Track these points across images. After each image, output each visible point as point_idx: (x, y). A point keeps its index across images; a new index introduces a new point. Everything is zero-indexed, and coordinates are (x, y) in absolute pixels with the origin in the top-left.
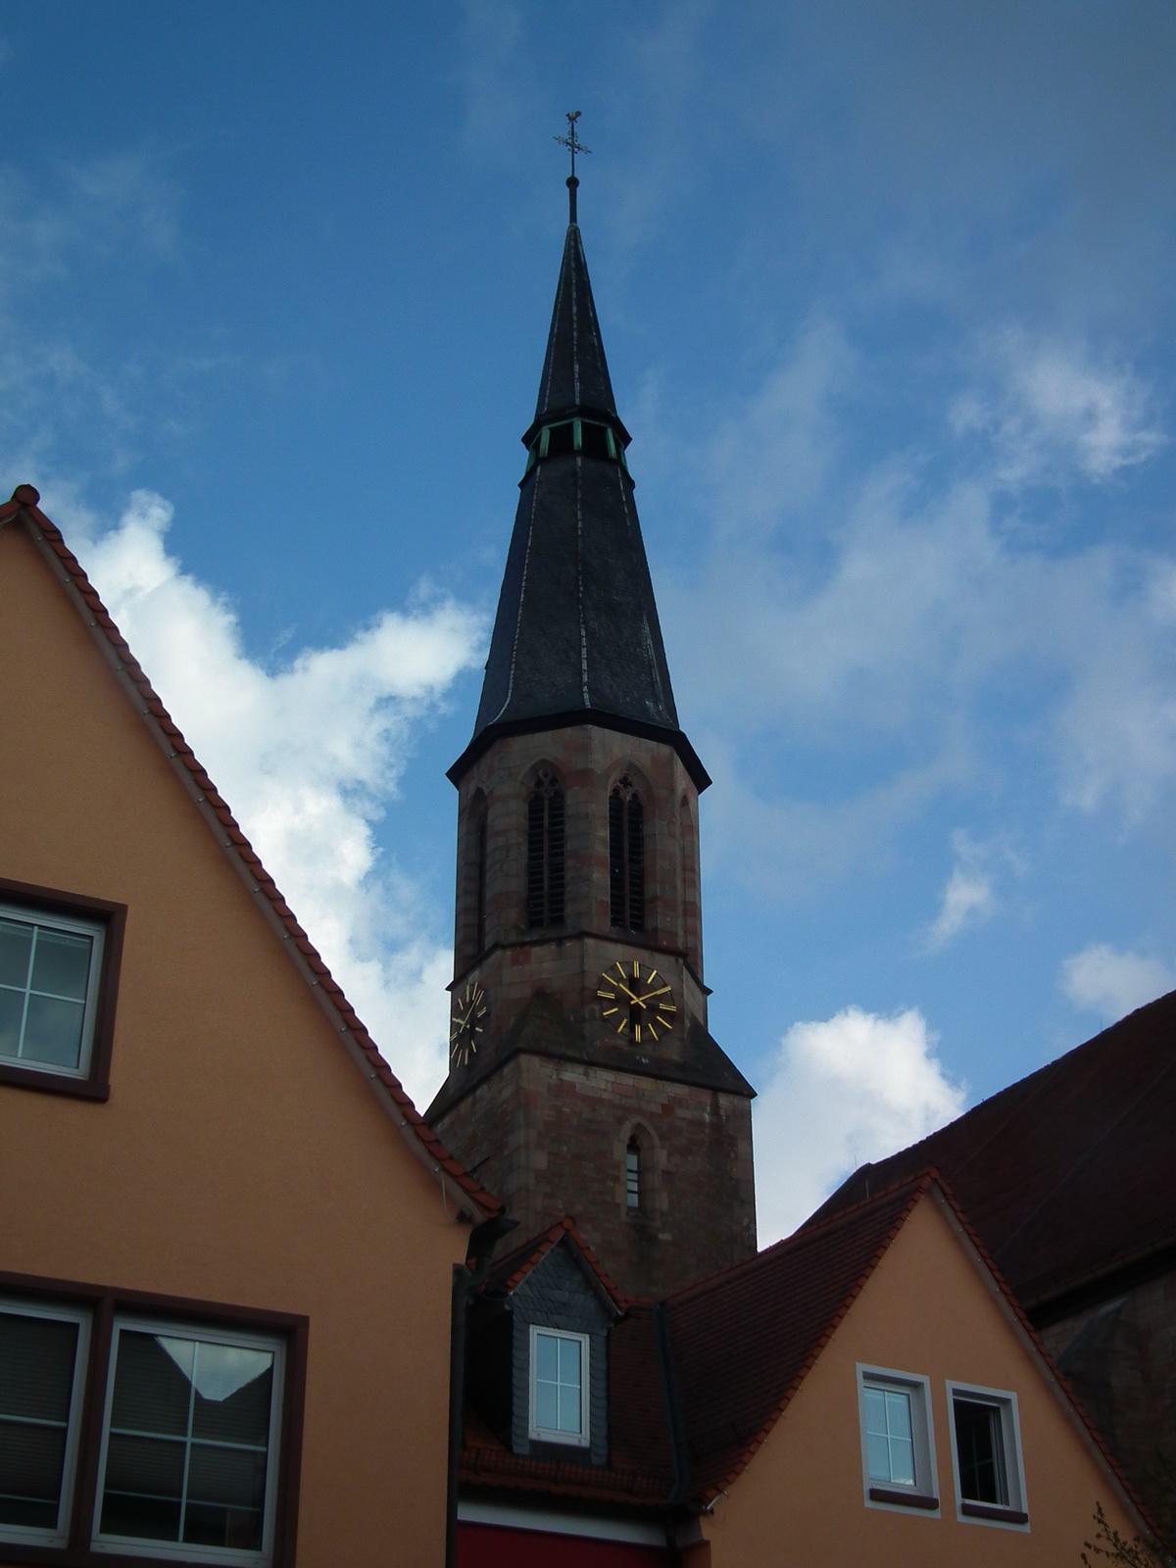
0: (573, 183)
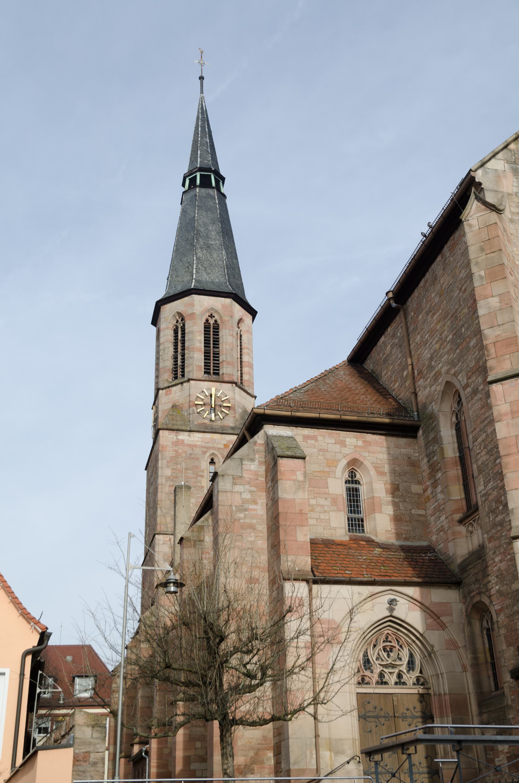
0: (201, 78)
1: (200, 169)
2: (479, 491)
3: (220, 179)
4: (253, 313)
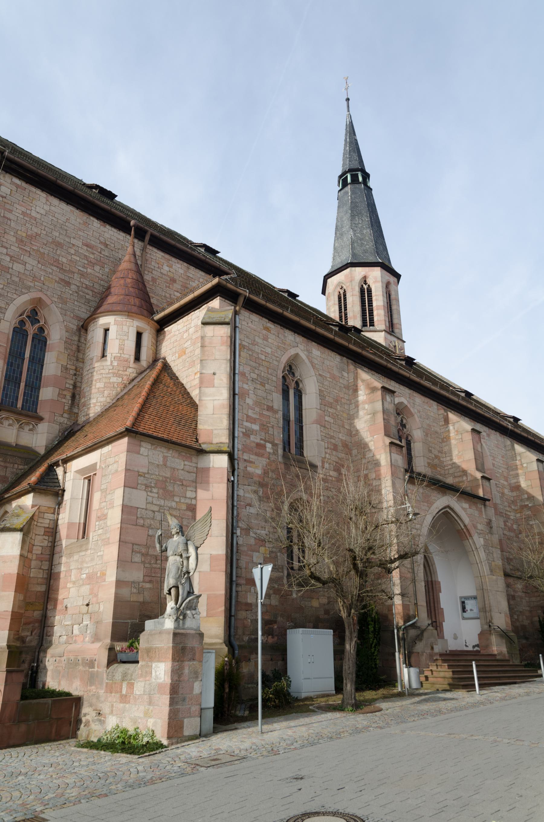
0: (348, 100)
1: (350, 171)
2: (470, 467)
3: (366, 176)
4: (398, 276)
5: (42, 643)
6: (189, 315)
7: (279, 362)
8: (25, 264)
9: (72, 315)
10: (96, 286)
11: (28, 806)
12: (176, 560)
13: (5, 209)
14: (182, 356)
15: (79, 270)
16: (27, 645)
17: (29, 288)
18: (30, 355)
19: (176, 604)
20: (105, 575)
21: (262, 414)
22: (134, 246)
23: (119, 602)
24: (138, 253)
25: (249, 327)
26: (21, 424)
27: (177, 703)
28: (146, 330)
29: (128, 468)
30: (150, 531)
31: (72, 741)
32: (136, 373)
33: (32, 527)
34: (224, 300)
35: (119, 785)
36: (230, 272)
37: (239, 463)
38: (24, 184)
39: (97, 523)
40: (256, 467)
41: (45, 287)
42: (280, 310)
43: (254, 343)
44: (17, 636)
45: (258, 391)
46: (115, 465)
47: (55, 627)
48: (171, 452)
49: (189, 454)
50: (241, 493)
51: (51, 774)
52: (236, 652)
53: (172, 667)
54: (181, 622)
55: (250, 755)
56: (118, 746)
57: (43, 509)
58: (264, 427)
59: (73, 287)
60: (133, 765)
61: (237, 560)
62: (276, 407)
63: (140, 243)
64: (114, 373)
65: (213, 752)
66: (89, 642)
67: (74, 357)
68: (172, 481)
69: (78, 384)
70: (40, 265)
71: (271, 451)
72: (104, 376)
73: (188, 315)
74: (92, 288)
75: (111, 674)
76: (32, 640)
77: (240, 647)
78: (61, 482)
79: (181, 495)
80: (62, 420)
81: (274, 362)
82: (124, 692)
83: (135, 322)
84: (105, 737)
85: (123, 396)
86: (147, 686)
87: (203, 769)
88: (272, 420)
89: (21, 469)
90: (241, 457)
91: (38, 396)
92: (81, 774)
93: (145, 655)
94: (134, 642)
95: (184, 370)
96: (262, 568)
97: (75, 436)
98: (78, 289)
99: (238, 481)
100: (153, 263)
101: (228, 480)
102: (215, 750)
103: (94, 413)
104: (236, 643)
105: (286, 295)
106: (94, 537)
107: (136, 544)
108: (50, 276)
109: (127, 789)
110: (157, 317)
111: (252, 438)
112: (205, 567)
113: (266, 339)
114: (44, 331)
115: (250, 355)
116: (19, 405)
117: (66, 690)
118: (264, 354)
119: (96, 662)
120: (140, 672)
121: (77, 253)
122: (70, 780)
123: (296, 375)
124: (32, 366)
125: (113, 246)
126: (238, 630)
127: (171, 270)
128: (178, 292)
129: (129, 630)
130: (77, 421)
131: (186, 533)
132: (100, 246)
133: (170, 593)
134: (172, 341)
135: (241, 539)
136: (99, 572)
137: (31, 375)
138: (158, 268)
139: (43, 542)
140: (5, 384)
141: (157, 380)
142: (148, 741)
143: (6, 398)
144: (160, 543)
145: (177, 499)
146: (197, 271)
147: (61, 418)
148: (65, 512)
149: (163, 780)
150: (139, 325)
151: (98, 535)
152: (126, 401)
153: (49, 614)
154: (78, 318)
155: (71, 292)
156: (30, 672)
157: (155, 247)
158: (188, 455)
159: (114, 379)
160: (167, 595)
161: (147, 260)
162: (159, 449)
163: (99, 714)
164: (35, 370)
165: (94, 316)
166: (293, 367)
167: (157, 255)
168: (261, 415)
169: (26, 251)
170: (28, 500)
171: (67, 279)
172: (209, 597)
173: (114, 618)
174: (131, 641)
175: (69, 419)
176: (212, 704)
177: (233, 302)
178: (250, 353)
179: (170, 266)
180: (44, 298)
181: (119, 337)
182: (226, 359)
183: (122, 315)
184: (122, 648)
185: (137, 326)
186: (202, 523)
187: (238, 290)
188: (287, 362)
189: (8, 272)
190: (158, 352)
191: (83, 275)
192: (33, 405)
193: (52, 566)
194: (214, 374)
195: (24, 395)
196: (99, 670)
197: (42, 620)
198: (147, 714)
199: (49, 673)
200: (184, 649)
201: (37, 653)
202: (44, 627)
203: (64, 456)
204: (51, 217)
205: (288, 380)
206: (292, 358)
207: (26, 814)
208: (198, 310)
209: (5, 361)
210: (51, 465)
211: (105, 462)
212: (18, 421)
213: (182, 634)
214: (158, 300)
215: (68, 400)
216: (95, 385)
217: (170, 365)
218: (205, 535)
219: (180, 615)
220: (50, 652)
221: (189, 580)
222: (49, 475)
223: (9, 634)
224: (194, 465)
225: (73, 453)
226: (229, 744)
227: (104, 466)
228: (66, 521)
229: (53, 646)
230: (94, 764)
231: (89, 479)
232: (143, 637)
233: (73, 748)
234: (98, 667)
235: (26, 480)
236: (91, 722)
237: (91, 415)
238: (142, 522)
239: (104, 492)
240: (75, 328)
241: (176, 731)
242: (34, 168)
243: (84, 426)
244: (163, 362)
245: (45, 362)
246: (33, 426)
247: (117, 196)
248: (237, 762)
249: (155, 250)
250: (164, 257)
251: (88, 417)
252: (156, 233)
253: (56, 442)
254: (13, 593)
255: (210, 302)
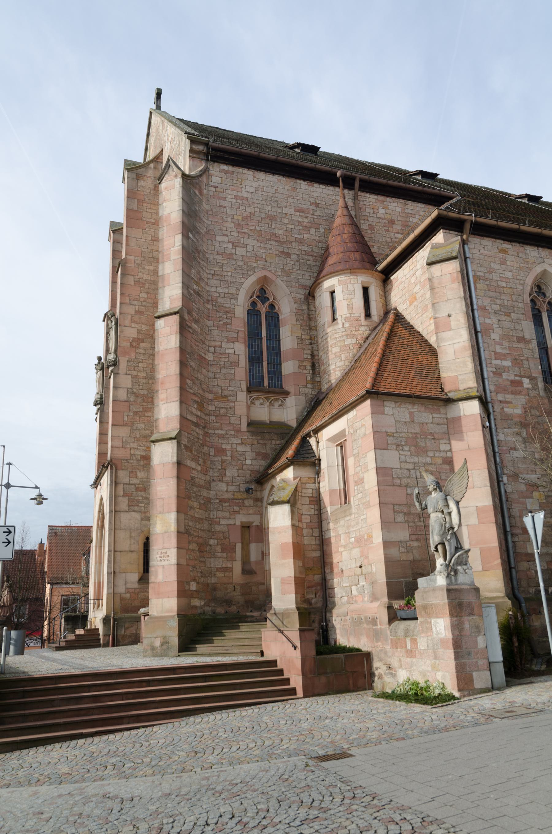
5: (327, 604)
6: (414, 257)
7: (523, 285)
8: (245, 246)
9: (298, 286)
10: (315, 250)
11: (336, 744)
12: (437, 517)
13: (219, 198)
14: (413, 302)
15: (296, 238)
16: (314, 606)
17: (253, 269)
18: (266, 334)
19: (445, 560)
20: (372, 537)
21: (512, 347)
22: (344, 198)
23: (389, 563)
24: (350, 203)
25: (482, 254)
26: (271, 402)
27: (462, 657)
28: (372, 283)
29: (375, 430)
30: (409, 489)
31: (369, 692)
32: (370, 330)
33: (297, 498)
34: (448, 231)
35: (414, 731)
36: (453, 195)
37: (494, 405)
38: (231, 168)
39: (356, 488)
40: (515, 407)
41: (268, 263)
42: (515, 226)
43: (491, 271)
44: (303, 599)
45: (504, 323)
46: (363, 429)
47: (335, 589)
48: (416, 407)
49: (437, 406)
50: (501, 437)
51: (353, 719)
52: (523, 605)
53: (451, 622)
54: (453, 578)
55: (548, 708)
56: (411, 697)
57: (304, 480)
58: (517, 362)
59: (293, 257)
60: (427, 714)
61: (509, 509)
62: (527, 336)
63: (350, 192)
64: (347, 335)
65: (508, 704)
66: (368, 601)
67: (307, 326)
68: (422, 437)
69: (316, 353)
70: (259, 244)
71: (530, 386)
72: (338, 340)
73: (412, 257)
74: (311, 253)
75: (393, 630)
76: (317, 602)
77: (527, 600)
78: (316, 451)
79: (434, 449)
80: (306, 391)
81: (518, 286)
82: (409, 647)
83: (358, 277)
84: (399, 689)
85: (360, 356)
86: (429, 641)
87: (497, 719)
88: (525, 351)
89: (279, 444)
90: (495, 398)
91: (281, 372)
92: (379, 720)
93: (423, 612)
94: (411, 600)
95: (417, 317)
96: (533, 517)
97: (321, 405)
98: (298, 257)
99: (495, 425)
100: (367, 210)
101: (483, 426)
102: (510, 702)
103: (335, 379)
104: (521, 596)
105: (526, 201)
106: (355, 502)
107: (396, 505)
108: (271, 252)
109: (423, 735)
110: (380, 267)
111: (505, 376)
112: (474, 520)
113: (503, 262)
114: (275, 307)
115: (487, 285)
116: (266, 383)
117: (356, 646)
118: (504, 280)
119: (378, 620)
120: (421, 628)
121: (291, 221)
122: (371, 725)
123: (547, 295)
124: (270, 344)
125: (324, 203)
126: (522, 583)
127: (388, 211)
128: (398, 233)
129: (404, 589)
130: (321, 389)
131: (444, 489)
132: (311, 207)
133: (437, 550)
134: (400, 289)
135: (510, 486)
136: (366, 535)
137: (271, 353)
138: (374, 213)
139: (310, 511)
140: (249, 366)
141: (391, 333)
142: (440, 693)
143: (253, 379)
144: (419, 501)
145: (431, 454)
146: (416, 204)
147: (306, 389)
148: (324, 480)
149: (457, 728)
150: (364, 280)
151: (359, 499)
152: (363, 362)
153: (328, 577)
154: (303, 287)
155: (292, 263)
156: (321, 631)
157: (367, 192)
158: (435, 407)
159: (349, 341)
160: (435, 552)
161: (360, 208)
162: (403, 405)
163: (390, 667)
164: (273, 347)
165: (318, 282)
166: (543, 287)
167: (370, 199)
168: (511, 348)
169: (244, 233)
170: (289, 473)
171: (286, 250)
172: (482, 551)
173: (387, 577)
174: (407, 599)
175: (314, 388)
176: (501, 658)
177: (458, 232)
178: (488, 283)
179: (386, 208)
180: (269, 275)
181: (345, 297)
182: (460, 297)
183: (345, 273)
184: (400, 606)
185: (362, 281)
186: (459, 476)
187: (462, 217)
188: (533, 283)
189: (233, 259)
190: (388, 304)
191: (300, 242)
192: (278, 381)
193: (322, 532)
194: (449, 316)
195: (268, 374)
196: (382, 627)
197: (322, 583)
198: (434, 668)
199: (338, 631)
200: (460, 605)
201: (324, 614)
202: (326, 590)
203: (314, 427)
204: (260, 193)
205: (538, 303)
206: (539, 277)
207: (335, 750)
208: (422, 249)
209: (245, 344)
210: (304, 437)
211: (353, 427)
212: (268, 399)
213: (456, 590)
214: (379, 248)
215: (308, 371)
216: (332, 351)
217: (403, 314)
218: (464, 488)
219: (451, 571)
220: (335, 612)
221: (455, 535)
222: (304, 447)
223: (296, 598)
224: (443, 416)
225: (321, 423)
226: (525, 697)
227: (352, 431)
228: (327, 489)
229: (337, 606)
230: (391, 712)
231: (341, 446)
232: (417, 594)
233: (370, 698)
234: (380, 625)
235: (285, 454)
236: (384, 675)
237: (333, 381)
238: (399, 482)
239: (356, 456)
240: (302, 297)
241: (466, 684)
242: (237, 149)
243: (328, 394)
244: (394, 313)
245: (281, 338)
246: (282, 402)
247: (320, 148)
248: (533, 714)
249: (367, 195)
250: (377, 199)
251: (330, 384)
252: (365, 177)
253: (306, 413)
254: (292, 560)
255: (433, 238)
